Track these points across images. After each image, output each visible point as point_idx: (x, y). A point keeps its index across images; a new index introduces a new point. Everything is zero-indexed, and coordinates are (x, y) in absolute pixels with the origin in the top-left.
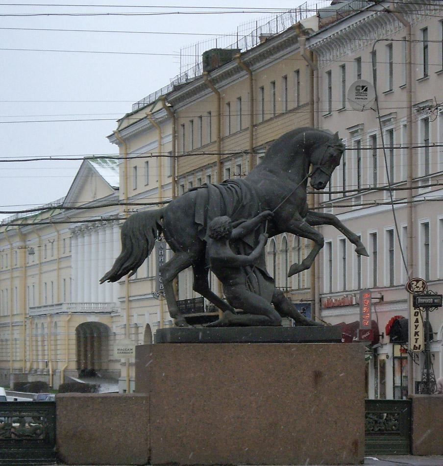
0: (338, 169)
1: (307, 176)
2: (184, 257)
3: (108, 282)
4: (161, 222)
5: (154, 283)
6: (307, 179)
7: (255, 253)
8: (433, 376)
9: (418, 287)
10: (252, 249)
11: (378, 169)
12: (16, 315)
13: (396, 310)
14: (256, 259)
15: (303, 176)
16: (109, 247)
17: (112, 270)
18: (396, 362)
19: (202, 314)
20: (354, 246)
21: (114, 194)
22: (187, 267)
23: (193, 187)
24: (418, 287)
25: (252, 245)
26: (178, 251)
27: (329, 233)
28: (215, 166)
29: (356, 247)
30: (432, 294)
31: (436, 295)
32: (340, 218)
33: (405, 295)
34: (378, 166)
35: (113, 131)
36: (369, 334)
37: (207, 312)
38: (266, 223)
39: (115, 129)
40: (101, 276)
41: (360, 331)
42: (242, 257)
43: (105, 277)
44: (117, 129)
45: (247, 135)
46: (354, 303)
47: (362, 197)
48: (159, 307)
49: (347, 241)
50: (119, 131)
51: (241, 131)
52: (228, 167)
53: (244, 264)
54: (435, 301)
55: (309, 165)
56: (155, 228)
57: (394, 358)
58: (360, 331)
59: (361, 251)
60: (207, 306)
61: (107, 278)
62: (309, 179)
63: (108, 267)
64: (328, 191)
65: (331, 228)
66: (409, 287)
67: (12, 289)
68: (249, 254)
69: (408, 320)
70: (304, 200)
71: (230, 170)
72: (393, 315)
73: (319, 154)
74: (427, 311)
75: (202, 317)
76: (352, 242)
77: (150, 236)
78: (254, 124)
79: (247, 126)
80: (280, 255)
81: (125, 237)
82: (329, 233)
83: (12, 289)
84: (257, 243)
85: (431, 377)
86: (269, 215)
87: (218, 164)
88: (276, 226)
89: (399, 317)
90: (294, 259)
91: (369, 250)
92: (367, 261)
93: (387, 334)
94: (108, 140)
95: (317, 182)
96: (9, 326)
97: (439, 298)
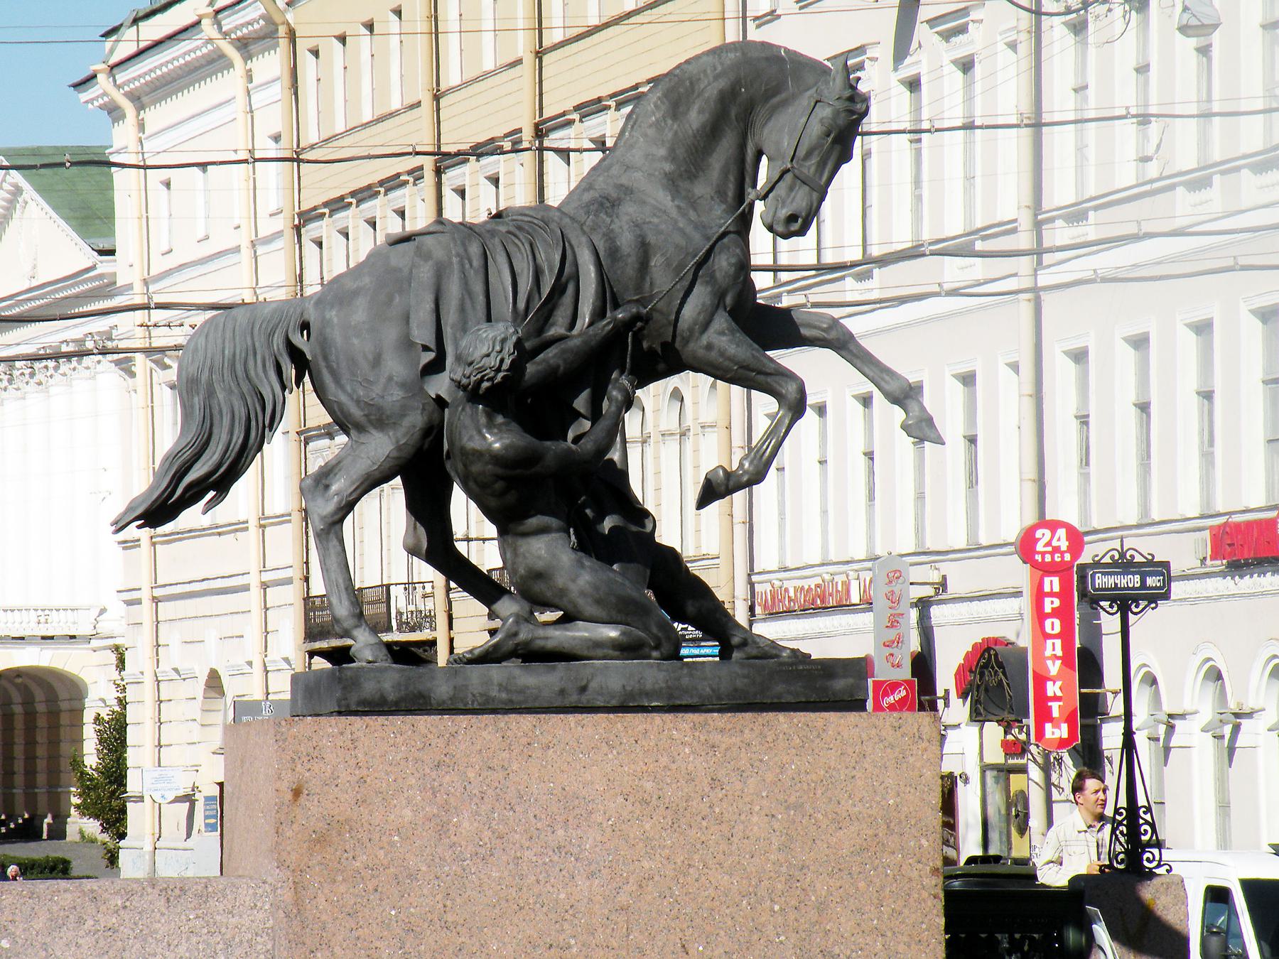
0: (849, 173)
1: (752, 196)
2: (380, 446)
3: (139, 527)
4: (299, 341)
6: (751, 205)
8: (1148, 817)
9: (1051, 543)
11: (925, 185)
13: (987, 620)
16: (125, 425)
17: (152, 489)
18: (990, 775)
20: (898, 414)
21: (93, 268)
22: (386, 479)
23: (409, 229)
24: (1057, 550)
26: (360, 428)
29: (904, 416)
30: (1138, 559)
31: (1151, 563)
32: (856, 326)
33: (1018, 574)
34: (925, 176)
36: (903, 693)
37: (399, 630)
40: (117, 507)
41: (878, 685)
43: (130, 509)
46: (855, 598)
47: (1091, 214)
48: (291, 608)
49: (878, 397)
54: (1150, 581)
55: (758, 160)
57: (984, 769)
58: (878, 685)
59: (922, 430)
60: (400, 613)
62: (759, 207)
63: (139, 483)
64: (771, 262)
65: (827, 356)
66: (1026, 547)
69: (1025, 650)
72: (978, 635)
73: (787, 131)
74: (1124, 611)
76: (896, 399)
77: (269, 386)
80: (671, 438)
81: (187, 388)
85: (1141, 821)
89: (996, 641)
90: (712, 455)
91: (951, 424)
92: (949, 456)
93: (963, 695)
95: (784, 213)
96: (246, 588)
97: (1163, 575)
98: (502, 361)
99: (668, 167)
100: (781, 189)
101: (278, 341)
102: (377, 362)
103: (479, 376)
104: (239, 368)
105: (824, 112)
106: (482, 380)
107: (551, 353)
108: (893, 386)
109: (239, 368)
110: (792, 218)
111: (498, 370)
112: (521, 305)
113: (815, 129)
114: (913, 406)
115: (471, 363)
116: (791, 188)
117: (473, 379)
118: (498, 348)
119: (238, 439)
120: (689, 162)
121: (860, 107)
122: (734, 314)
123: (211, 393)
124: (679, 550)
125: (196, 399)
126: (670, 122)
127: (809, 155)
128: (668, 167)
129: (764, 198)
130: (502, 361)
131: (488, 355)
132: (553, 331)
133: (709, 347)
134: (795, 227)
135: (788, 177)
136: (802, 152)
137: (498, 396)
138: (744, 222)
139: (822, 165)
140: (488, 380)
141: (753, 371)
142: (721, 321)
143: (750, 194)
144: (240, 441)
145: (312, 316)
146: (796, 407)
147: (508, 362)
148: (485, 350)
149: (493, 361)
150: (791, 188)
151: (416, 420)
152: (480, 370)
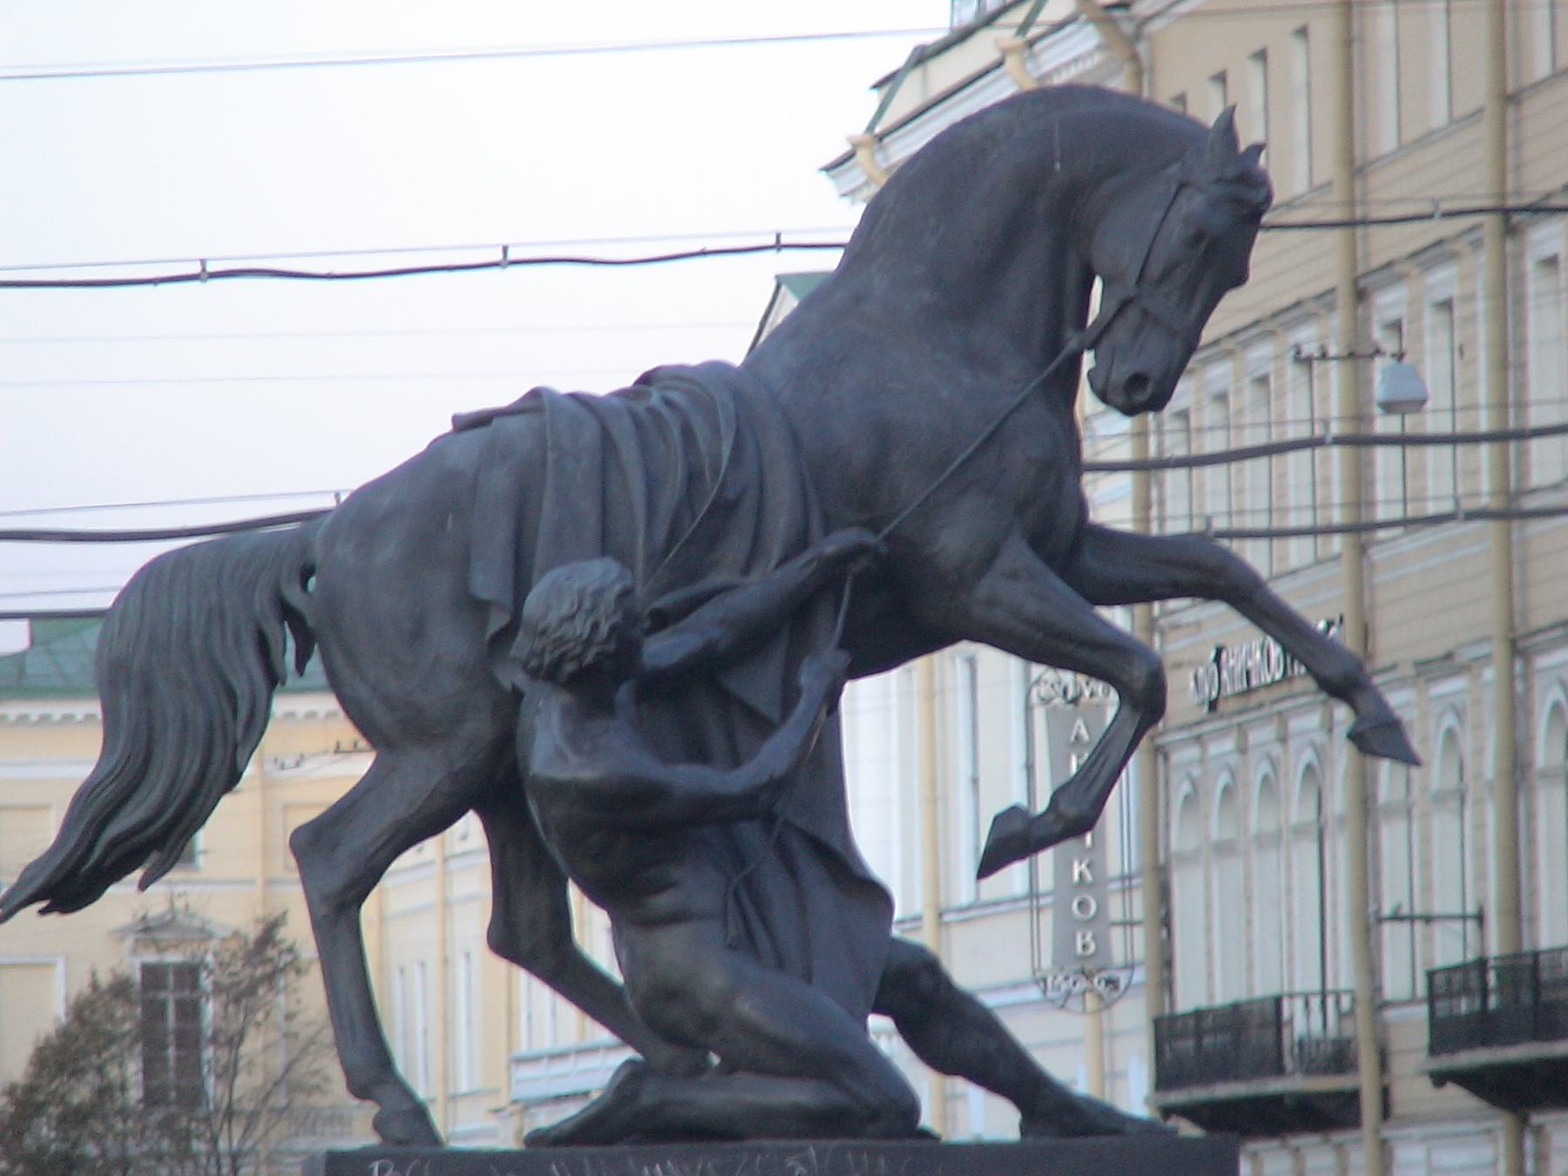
2: (425, 772)
3: (43, 912)
4: (294, 596)
5: (1047, 920)
6: (1075, 361)
7: (773, 756)
10: (764, 727)
12: (465, 1095)
14: (778, 785)
15: (1054, 343)
19: (1274, 1086)
22: (435, 822)
25: (773, 713)
27: (1195, 640)
28: (1331, 307)
35: (849, 139)
38: (842, 590)
39: (859, 128)
42: (687, 777)
44: (871, 128)
45: (1481, 135)
50: (881, 138)
51: (1459, 122)
52: (1392, 315)
53: (714, 815)
56: (271, 627)
61: (29, 891)
62: (1088, 360)
65: (1217, 621)
67: (445, 961)
68: (736, 761)
70: (1065, 460)
71: (1405, 328)
75: (1276, 1100)
77: (246, 671)
78: (1511, 87)
79: (1473, 105)
80: (923, 758)
82: (1195, 640)
83: (445, 961)
84: (789, 696)
86: (861, 550)
87: (1343, 298)
88: (898, 617)
94: (826, 183)
95: (1122, 372)
98: (595, 627)
99: (926, 296)
100: (1121, 333)
101: (261, 600)
102: (418, 633)
103: (557, 653)
104: (197, 642)
105: (1193, 203)
106: (561, 660)
107: (708, 614)
108: (1332, 670)
109: (197, 642)
110: (1137, 381)
111: (588, 643)
112: (661, 535)
113: (1176, 231)
114: (1366, 704)
115: (543, 633)
116: (1137, 332)
117: (548, 658)
118: (587, 604)
119: (192, 767)
120: (966, 294)
121: (1257, 196)
122: (1036, 542)
123: (148, 689)
124: (116, 594)
125: (124, 699)
126: (933, 221)
127: (1165, 275)
128: (926, 296)
129: (1093, 346)
130: (595, 627)
131: (572, 617)
132: (716, 579)
133: (991, 603)
134: (1141, 397)
135: (1133, 315)
136: (1155, 270)
137: (597, 677)
138: (1063, 386)
139: (1190, 289)
140: (572, 659)
141: (1071, 640)
142: (1017, 553)
143: (1072, 341)
144: (195, 768)
145: (318, 555)
146: (1146, 702)
147: (604, 628)
148: (565, 609)
149: (581, 628)
150: (1137, 332)
151: (479, 727)
152: (561, 641)
